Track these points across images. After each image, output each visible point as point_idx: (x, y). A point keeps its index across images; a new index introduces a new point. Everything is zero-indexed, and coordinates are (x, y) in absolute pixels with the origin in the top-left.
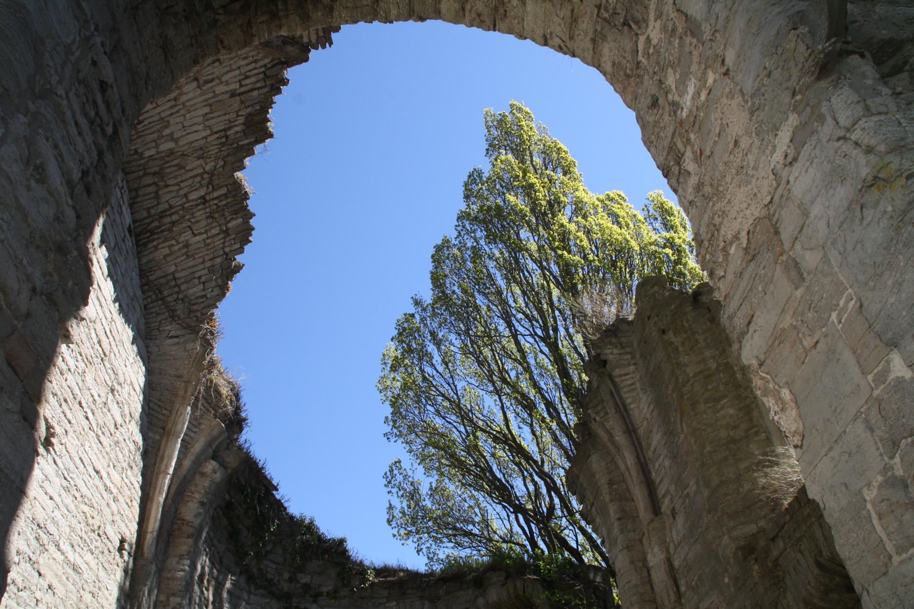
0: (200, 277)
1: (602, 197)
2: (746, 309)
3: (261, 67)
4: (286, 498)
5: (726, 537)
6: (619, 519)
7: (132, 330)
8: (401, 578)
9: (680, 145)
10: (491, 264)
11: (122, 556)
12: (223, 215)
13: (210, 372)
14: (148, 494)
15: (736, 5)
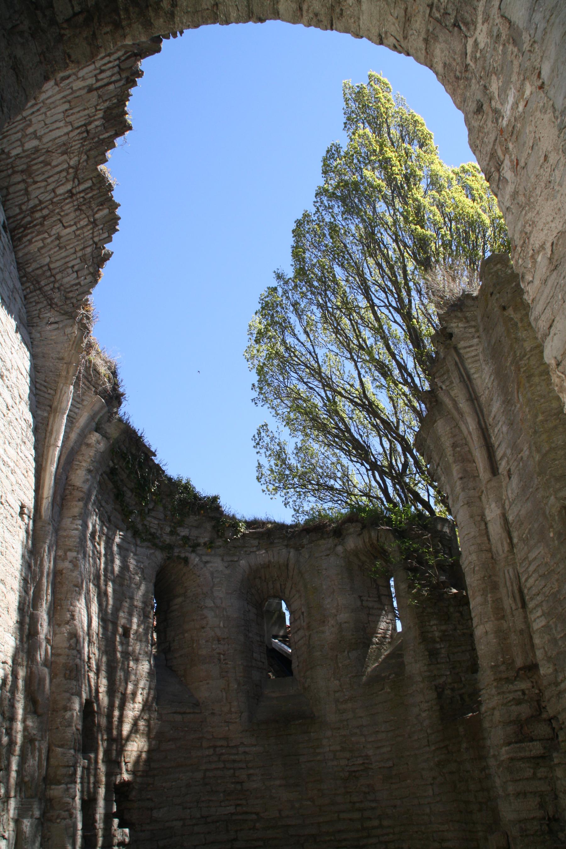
0: (73, 267)
1: (457, 169)
2: (548, 314)
3: (115, 60)
4: (164, 463)
5: (552, 497)
6: (461, 478)
7: (15, 320)
8: (269, 530)
9: (500, 153)
10: (348, 240)
11: (23, 519)
12: (90, 207)
13: (88, 353)
14: (41, 465)
15: (554, 16)
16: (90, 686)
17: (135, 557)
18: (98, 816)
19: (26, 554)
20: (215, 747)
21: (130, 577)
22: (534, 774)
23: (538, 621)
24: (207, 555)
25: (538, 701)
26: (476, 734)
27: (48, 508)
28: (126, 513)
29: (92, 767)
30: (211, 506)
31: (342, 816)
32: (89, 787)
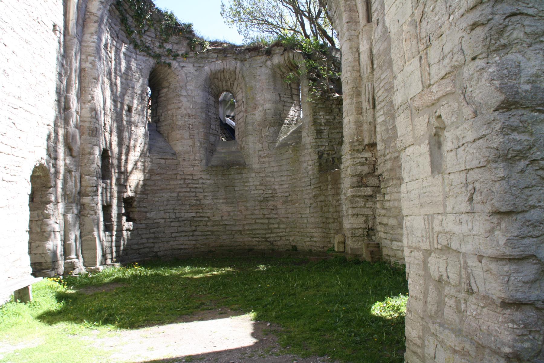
6: (348, 22)
11: (56, 34)
16: (106, 141)
17: (136, 62)
18: (113, 215)
19: (60, 57)
20: (185, 179)
21: (132, 74)
22: (365, 205)
23: (380, 117)
24: (183, 62)
25: (374, 165)
26: (337, 182)
27: (73, 27)
28: (129, 33)
29: (109, 187)
30: (186, 32)
31: (257, 221)
32: (107, 199)
